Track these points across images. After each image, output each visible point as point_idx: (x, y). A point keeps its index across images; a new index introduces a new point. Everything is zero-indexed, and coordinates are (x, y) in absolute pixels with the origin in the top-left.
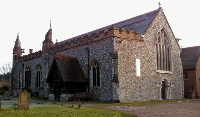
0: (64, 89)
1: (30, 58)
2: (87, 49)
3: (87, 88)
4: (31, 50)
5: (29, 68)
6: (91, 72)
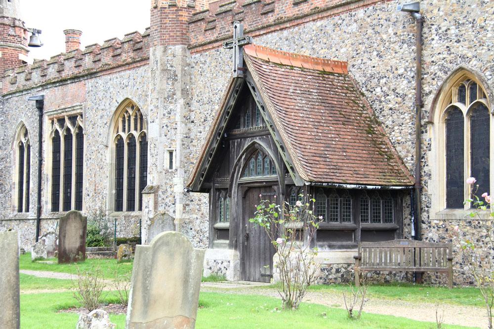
0: (226, 220)
1: (76, 71)
2: (412, 12)
3: (408, 219)
4: (71, 35)
5: (73, 119)
6: (437, 135)
